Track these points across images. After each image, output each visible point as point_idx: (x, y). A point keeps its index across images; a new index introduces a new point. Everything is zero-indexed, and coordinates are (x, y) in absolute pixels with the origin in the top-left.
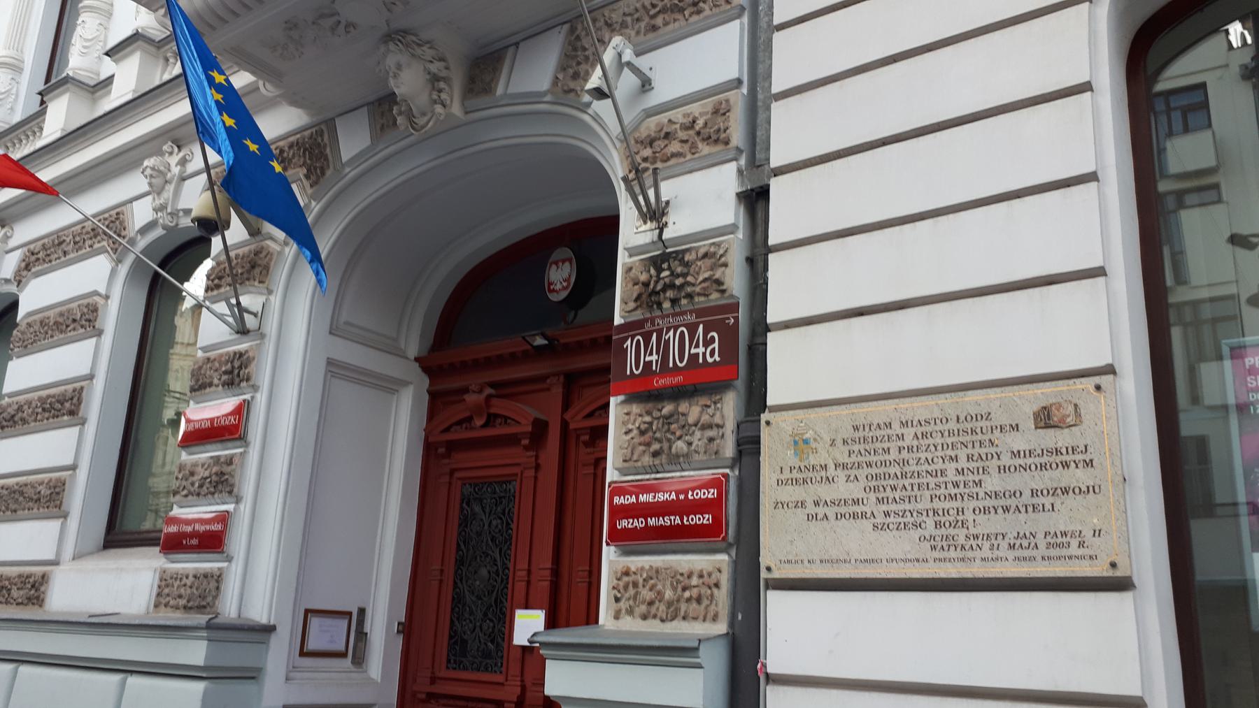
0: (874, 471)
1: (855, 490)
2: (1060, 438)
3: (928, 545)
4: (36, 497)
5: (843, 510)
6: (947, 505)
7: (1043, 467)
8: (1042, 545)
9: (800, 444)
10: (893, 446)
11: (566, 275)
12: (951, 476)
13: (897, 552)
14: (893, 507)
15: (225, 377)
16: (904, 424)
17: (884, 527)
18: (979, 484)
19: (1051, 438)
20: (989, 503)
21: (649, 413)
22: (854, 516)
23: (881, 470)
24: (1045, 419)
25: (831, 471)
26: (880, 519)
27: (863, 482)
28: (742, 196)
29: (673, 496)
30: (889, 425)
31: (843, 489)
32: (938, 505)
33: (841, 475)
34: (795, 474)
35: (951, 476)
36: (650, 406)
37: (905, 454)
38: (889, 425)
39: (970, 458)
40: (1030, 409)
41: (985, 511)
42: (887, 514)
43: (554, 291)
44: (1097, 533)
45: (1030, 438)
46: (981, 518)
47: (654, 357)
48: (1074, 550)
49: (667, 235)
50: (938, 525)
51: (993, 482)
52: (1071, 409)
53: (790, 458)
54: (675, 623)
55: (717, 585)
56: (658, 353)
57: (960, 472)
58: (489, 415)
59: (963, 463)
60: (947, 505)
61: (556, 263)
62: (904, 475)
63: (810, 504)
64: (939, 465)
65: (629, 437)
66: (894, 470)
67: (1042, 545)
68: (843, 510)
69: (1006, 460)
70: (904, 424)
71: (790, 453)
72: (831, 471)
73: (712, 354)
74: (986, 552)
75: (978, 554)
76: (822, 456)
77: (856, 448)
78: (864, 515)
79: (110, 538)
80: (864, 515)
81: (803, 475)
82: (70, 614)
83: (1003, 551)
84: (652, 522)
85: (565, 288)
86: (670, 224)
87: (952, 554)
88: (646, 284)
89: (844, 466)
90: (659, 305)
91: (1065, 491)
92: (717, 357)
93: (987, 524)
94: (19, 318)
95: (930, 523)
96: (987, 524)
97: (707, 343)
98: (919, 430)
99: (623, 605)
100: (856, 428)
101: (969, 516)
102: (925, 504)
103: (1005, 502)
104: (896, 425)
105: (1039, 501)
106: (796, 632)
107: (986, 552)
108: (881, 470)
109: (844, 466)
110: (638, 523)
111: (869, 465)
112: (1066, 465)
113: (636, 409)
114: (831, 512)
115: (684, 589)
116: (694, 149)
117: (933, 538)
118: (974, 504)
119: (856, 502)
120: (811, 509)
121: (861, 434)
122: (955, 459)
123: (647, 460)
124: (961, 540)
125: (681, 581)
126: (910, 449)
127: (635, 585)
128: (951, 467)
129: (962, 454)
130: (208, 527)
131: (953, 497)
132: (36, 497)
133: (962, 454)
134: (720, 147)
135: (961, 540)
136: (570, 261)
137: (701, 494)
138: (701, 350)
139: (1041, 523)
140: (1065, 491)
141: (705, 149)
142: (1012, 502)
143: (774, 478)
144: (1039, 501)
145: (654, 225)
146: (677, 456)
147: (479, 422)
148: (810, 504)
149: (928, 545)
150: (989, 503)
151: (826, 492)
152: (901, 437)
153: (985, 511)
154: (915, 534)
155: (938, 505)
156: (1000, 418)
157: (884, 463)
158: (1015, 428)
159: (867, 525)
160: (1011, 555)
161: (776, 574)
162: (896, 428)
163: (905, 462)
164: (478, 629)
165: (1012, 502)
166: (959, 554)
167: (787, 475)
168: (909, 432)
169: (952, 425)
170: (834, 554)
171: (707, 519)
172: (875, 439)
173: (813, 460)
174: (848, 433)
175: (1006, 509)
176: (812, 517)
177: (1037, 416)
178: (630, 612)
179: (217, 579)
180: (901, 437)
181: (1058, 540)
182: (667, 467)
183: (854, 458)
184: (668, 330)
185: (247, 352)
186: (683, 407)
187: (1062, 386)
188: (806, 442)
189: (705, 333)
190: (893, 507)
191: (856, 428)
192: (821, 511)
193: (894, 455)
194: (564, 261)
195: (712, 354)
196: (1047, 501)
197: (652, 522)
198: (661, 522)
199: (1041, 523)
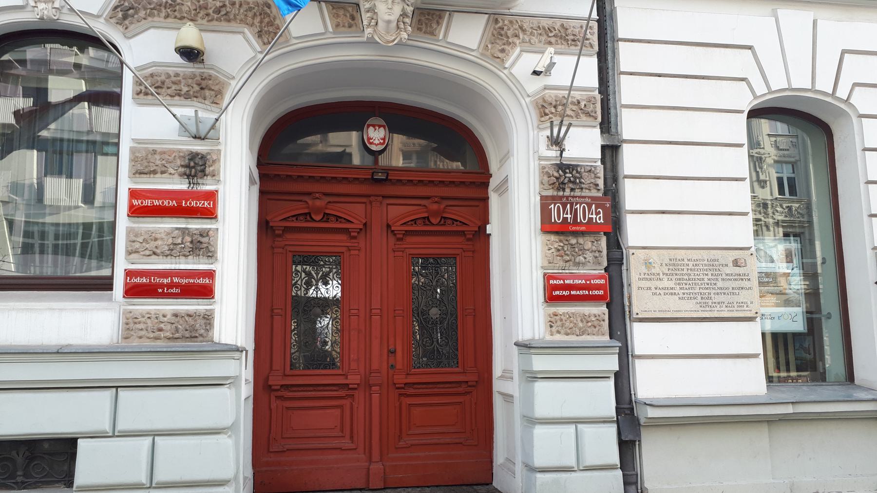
1: (671, 284)
2: (740, 270)
5: (667, 291)
7: (735, 280)
9: (648, 264)
12: (706, 281)
13: (688, 308)
14: (686, 291)
15: (182, 170)
16: (689, 260)
17: (683, 298)
18: (715, 284)
19: (737, 270)
20: (719, 291)
21: (561, 241)
22: (671, 294)
24: (736, 263)
25: (661, 276)
26: (681, 296)
27: (674, 281)
28: (603, 148)
29: (584, 282)
30: (683, 260)
31: (666, 283)
32: (701, 291)
34: (646, 276)
35: (706, 281)
36: (562, 238)
37: (689, 272)
38: (683, 260)
39: (712, 275)
40: (731, 259)
41: (718, 294)
44: (752, 303)
47: (569, 216)
48: (745, 308)
50: (702, 298)
51: (720, 284)
53: (644, 270)
57: (709, 280)
59: (710, 276)
61: (374, 126)
64: (702, 277)
66: (686, 277)
68: (667, 291)
69: (724, 276)
70: (689, 260)
72: (661, 276)
73: (600, 219)
76: (656, 270)
78: (675, 294)
80: (675, 294)
81: (649, 277)
84: (573, 293)
85: (381, 144)
88: (557, 178)
89: (667, 274)
93: (718, 298)
94: (299, 141)
95: (699, 297)
96: (718, 298)
97: (597, 213)
99: (554, 329)
102: (697, 291)
103: (723, 291)
109: (667, 274)
110: (566, 293)
113: (553, 238)
114: (662, 292)
115: (588, 322)
116: (577, 116)
119: (672, 289)
122: (707, 275)
123: (562, 264)
125: (585, 318)
127: (561, 320)
129: (710, 273)
131: (707, 289)
134: (591, 119)
136: (384, 127)
137: (598, 282)
138: (594, 216)
139: (735, 299)
141: (583, 117)
142: (726, 291)
145: (558, 148)
146: (579, 263)
147: (318, 217)
150: (719, 291)
151: (660, 284)
152: (688, 265)
153: (718, 294)
154: (694, 301)
155: (701, 291)
156: (722, 261)
157: (682, 274)
158: (727, 265)
159: (676, 297)
160: (726, 309)
161: (640, 316)
162: (686, 262)
163: (690, 275)
165: (726, 291)
168: (691, 263)
169: (706, 262)
170: (664, 308)
171: (601, 292)
173: (653, 271)
174: (667, 261)
178: (558, 332)
179: (208, 319)
180: (688, 265)
184: (576, 204)
185: (208, 154)
186: (581, 240)
188: (650, 263)
189: (596, 209)
190: (686, 291)
192: (658, 291)
194: (380, 126)
195: (600, 219)
196: (737, 291)
197: (573, 293)
198: (578, 293)
199: (735, 299)
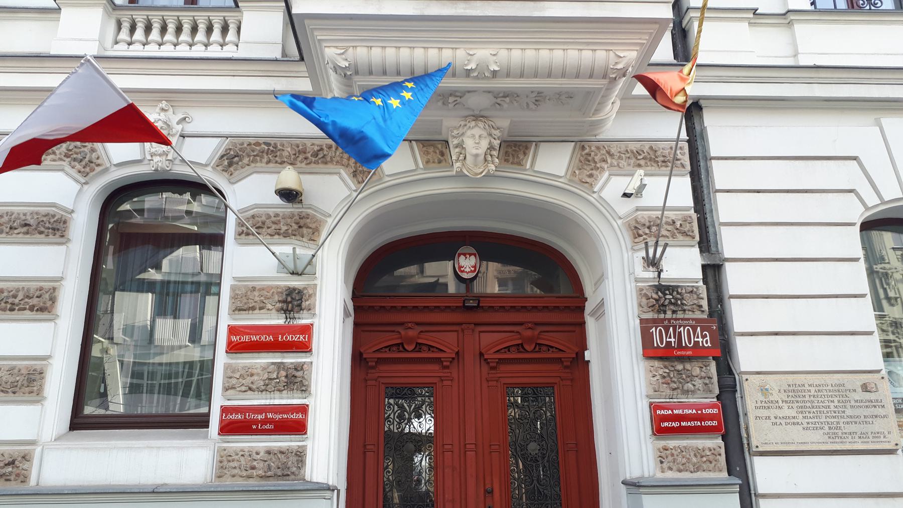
0: (800, 405)
1: (792, 413)
2: (872, 396)
3: (827, 436)
4: (23, 382)
5: (788, 421)
6: (833, 420)
7: (867, 407)
8: (871, 437)
10: (807, 394)
11: (473, 263)
12: (832, 408)
13: (815, 439)
14: (810, 420)
17: (808, 429)
19: (867, 396)
21: (666, 367)
22: (794, 424)
23: (803, 404)
24: (865, 388)
26: (805, 425)
29: (694, 411)
32: (828, 420)
33: (785, 406)
34: (763, 404)
35: (832, 408)
37: (812, 398)
39: (839, 401)
40: (859, 384)
41: (848, 423)
42: (808, 423)
43: (463, 271)
44: (889, 433)
45: (860, 395)
46: (846, 426)
47: (673, 340)
48: (882, 439)
49: (663, 275)
50: (830, 428)
51: (849, 412)
52: (873, 385)
54: (699, 473)
55: (720, 455)
56: (675, 337)
57: (836, 407)
58: (417, 343)
59: (836, 404)
60: (833, 420)
61: (465, 255)
62: (813, 407)
63: (772, 418)
64: (827, 404)
65: (655, 379)
66: (808, 404)
67: (871, 437)
68: (788, 421)
69: (853, 403)
71: (760, 394)
72: (780, 404)
74: (850, 440)
75: (847, 440)
77: (790, 394)
78: (798, 423)
79: (76, 421)
80: (798, 423)
81: (768, 405)
82: (98, 486)
83: (857, 439)
84: (683, 424)
85: (472, 271)
86: (664, 270)
87: (837, 440)
88: (656, 300)
89: (786, 402)
90: (665, 312)
91: (876, 417)
92: (709, 344)
95: (826, 427)
97: (704, 337)
98: (817, 389)
99: (665, 465)
100: (789, 386)
101: (842, 425)
103: (854, 420)
104: (806, 386)
105: (868, 420)
106: (766, 474)
107: (850, 440)
108: (803, 404)
109: (786, 402)
111: (797, 402)
112: (875, 407)
113: (657, 363)
114: (783, 422)
117: (828, 433)
118: (843, 420)
119: (794, 418)
120: (773, 420)
121: (791, 388)
123: (669, 392)
124: (840, 435)
125: (698, 453)
126: (814, 396)
127: (672, 455)
128: (832, 405)
129: (836, 400)
130: (285, 416)
131: (834, 417)
132: (23, 382)
133: (836, 400)
135: (840, 435)
136: (475, 255)
137: (710, 411)
138: (700, 340)
139: (869, 428)
140: (876, 417)
143: (754, 405)
144: (868, 420)
145: (654, 269)
147: (410, 348)
148: (772, 418)
149: (827, 436)
151: (780, 413)
152: (810, 391)
153: (848, 423)
154: (821, 432)
155: (828, 420)
158: (855, 391)
159: (800, 428)
160: (860, 440)
161: (760, 449)
162: (807, 387)
163: (813, 402)
164: (535, 482)
166: (839, 440)
167: (759, 404)
169: (830, 387)
170: (787, 440)
171: (715, 423)
172: (798, 391)
173: (771, 398)
175: (856, 423)
176: (774, 424)
177: (862, 386)
178: (670, 469)
179: (300, 456)
181: (876, 435)
182: (679, 396)
183: (790, 399)
186: (688, 366)
187: (870, 376)
188: (767, 390)
190: (810, 420)
191: (789, 386)
192: (778, 421)
193: (807, 398)
194: (470, 255)
196: (870, 420)
197: (683, 424)
199: (869, 428)
